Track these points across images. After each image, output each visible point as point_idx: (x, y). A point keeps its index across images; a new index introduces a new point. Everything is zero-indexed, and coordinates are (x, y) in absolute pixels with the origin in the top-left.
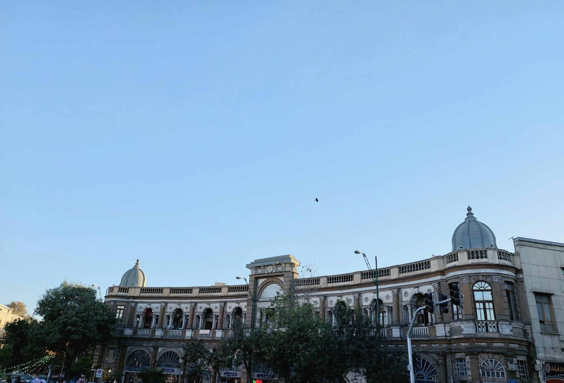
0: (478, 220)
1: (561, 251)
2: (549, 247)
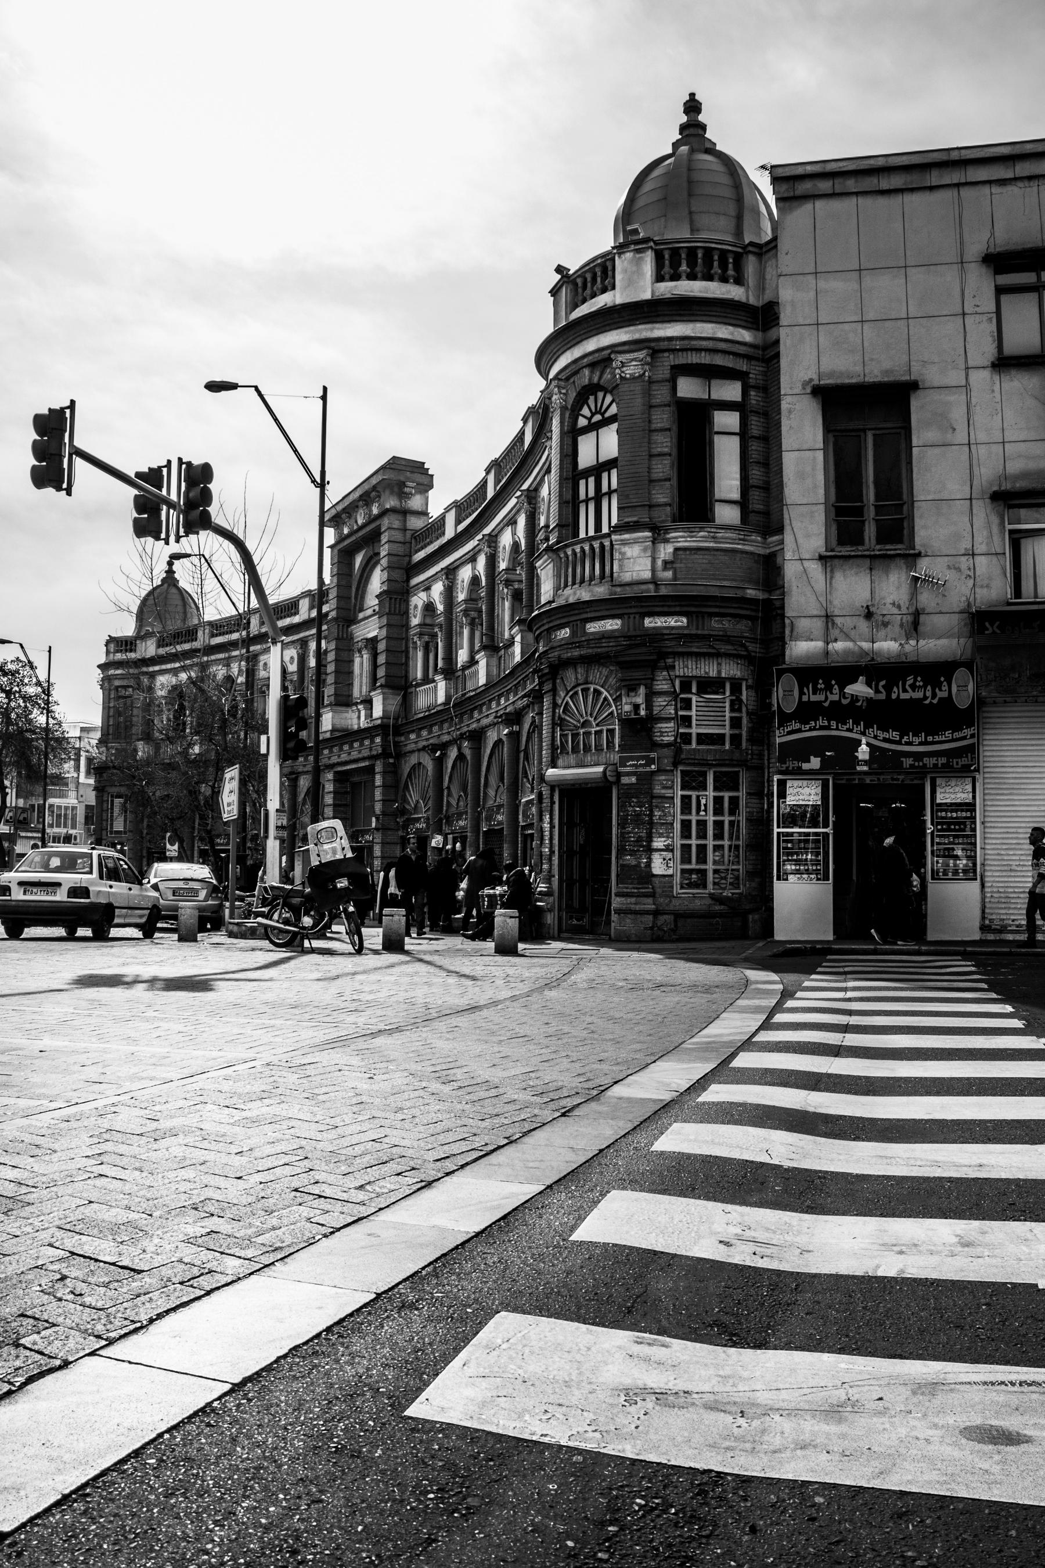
0: (718, 148)
1: (1002, 182)
2: (935, 178)
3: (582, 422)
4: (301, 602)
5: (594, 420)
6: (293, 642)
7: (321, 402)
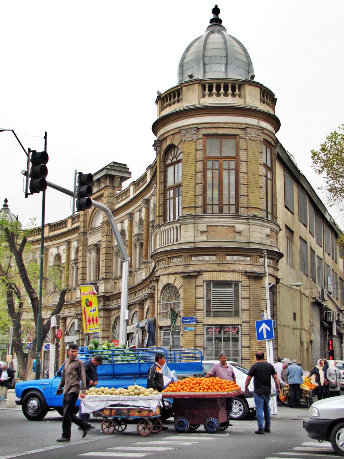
3: (169, 162)
4: (68, 221)
5: (173, 161)
6: (63, 242)
7: (44, 139)
